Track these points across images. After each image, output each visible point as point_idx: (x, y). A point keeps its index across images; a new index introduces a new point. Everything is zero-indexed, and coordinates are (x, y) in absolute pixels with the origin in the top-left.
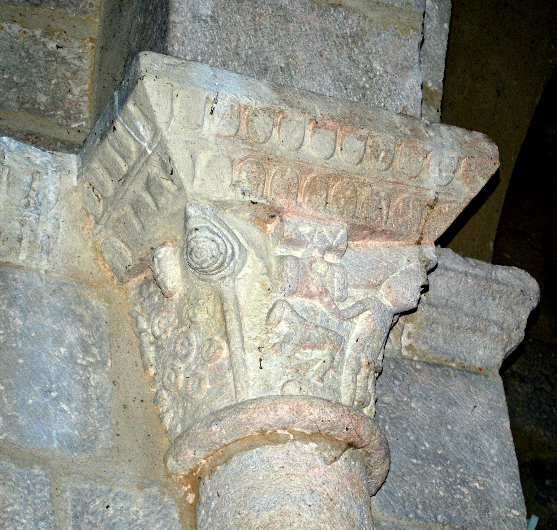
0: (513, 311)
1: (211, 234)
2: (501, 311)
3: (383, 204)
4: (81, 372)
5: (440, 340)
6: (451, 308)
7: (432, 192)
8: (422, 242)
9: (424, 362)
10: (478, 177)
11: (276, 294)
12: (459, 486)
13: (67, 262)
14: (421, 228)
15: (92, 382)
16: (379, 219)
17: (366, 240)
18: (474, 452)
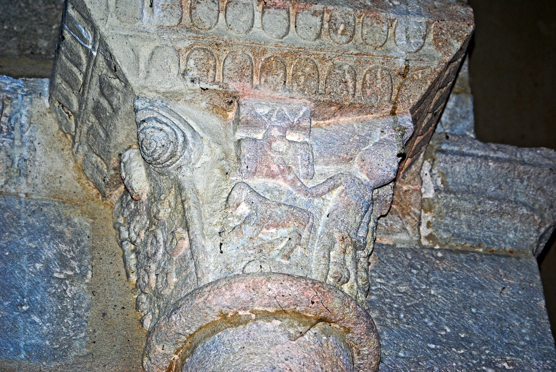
0: (544, 191)
1: (158, 123)
2: (531, 192)
3: (348, 76)
4: (56, 285)
5: (464, 226)
6: (473, 193)
7: (401, 60)
8: (396, 112)
9: (446, 250)
10: (451, 39)
11: (235, 178)
12: (484, 368)
13: (48, 184)
14: (393, 98)
15: (69, 294)
16: (345, 92)
17: (337, 118)
18: (503, 333)
